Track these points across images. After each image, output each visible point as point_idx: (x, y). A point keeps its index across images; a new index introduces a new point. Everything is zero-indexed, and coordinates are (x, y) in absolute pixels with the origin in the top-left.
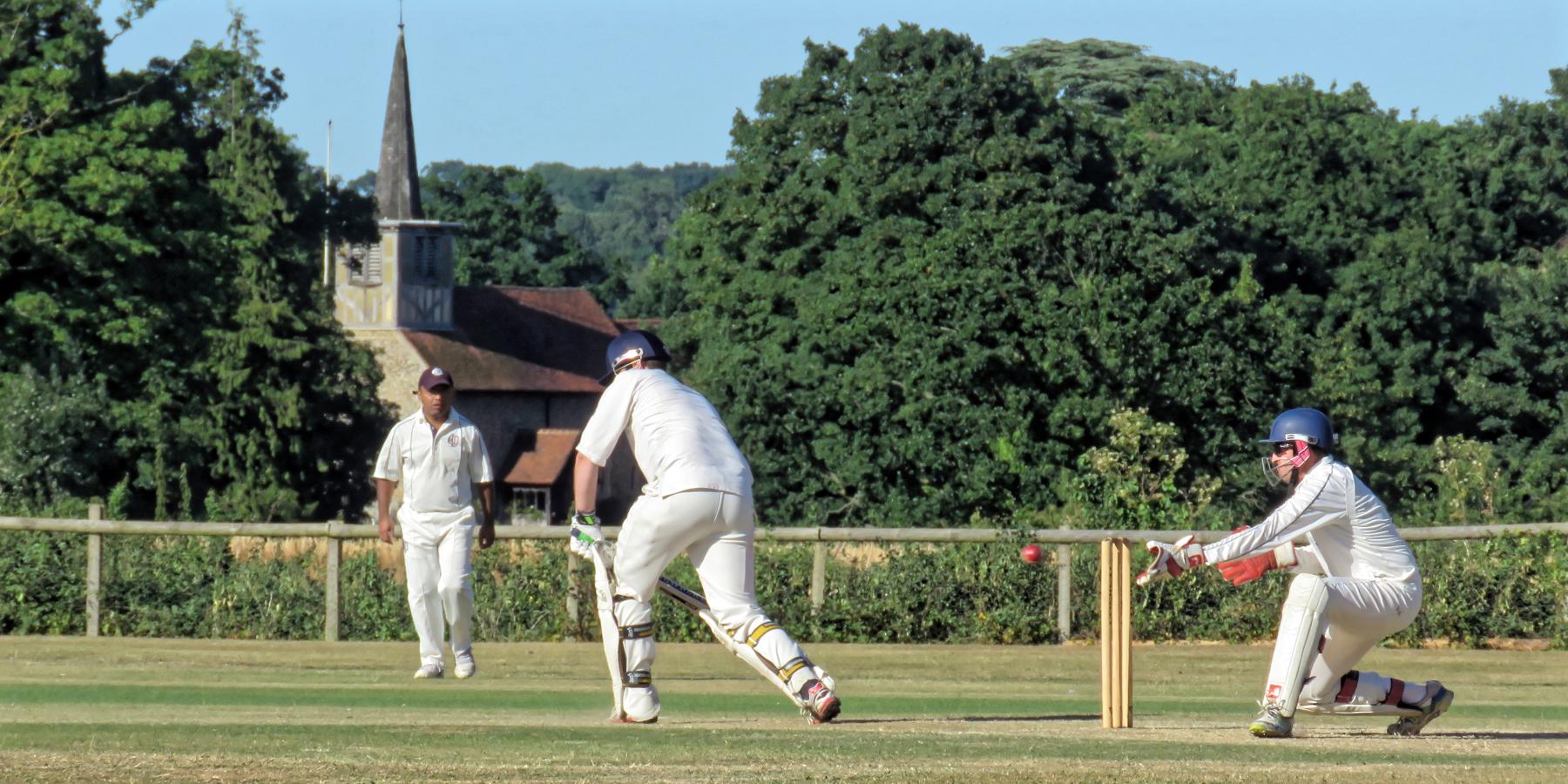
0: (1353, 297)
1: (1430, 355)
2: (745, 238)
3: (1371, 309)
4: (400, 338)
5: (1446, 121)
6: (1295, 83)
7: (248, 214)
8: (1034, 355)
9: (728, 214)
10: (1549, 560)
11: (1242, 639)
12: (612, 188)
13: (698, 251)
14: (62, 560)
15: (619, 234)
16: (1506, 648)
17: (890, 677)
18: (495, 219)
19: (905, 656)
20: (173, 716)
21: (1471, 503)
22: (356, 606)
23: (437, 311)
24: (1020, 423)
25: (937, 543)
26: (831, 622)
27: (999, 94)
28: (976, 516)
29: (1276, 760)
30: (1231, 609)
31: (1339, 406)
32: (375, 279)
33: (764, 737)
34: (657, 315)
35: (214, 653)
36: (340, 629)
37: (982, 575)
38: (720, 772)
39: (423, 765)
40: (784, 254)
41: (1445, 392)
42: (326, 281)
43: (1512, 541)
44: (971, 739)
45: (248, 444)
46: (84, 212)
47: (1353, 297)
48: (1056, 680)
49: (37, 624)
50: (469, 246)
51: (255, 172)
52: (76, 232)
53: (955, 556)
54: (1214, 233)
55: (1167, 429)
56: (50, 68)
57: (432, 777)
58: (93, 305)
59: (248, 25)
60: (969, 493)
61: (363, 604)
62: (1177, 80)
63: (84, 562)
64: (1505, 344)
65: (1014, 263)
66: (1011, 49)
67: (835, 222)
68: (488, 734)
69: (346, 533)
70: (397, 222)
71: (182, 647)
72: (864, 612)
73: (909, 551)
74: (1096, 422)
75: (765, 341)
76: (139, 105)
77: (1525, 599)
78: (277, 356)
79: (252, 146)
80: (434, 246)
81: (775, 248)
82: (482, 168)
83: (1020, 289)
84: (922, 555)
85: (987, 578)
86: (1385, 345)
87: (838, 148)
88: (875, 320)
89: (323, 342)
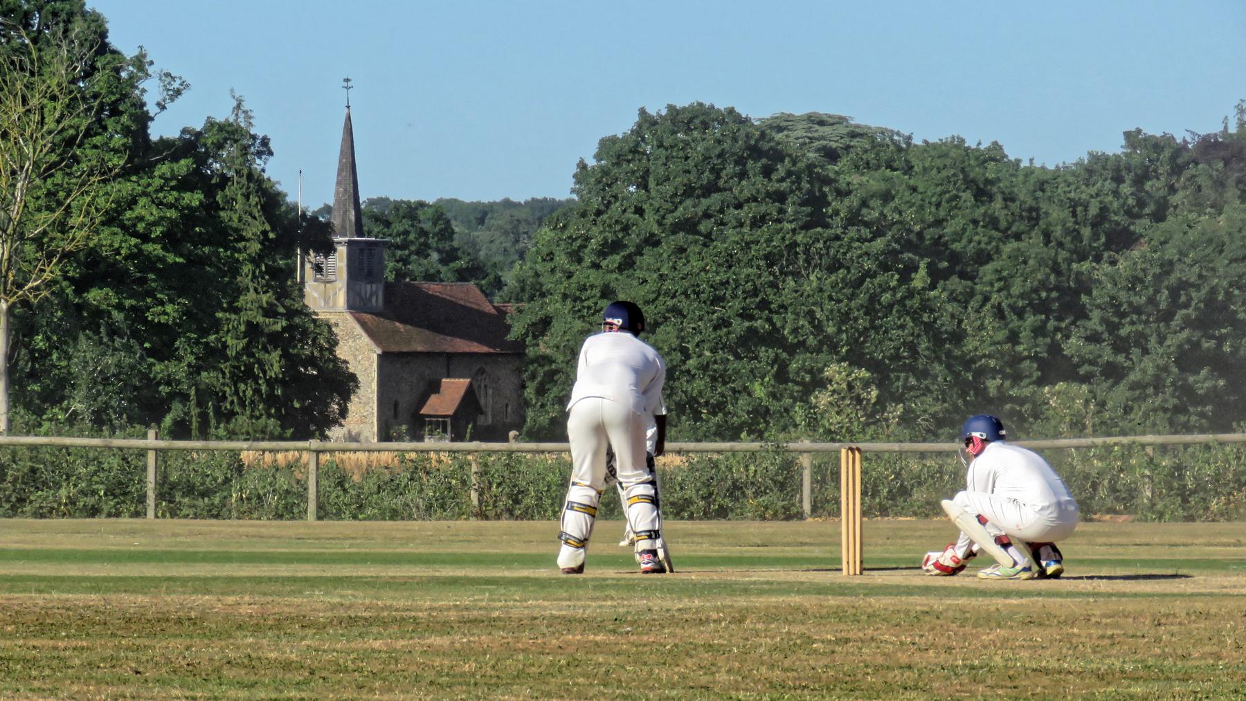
0: (992, 285)
1: (1045, 323)
2: (583, 247)
4: (349, 317)
7: (248, 234)
8: (779, 324)
9: (571, 231)
10: (1133, 461)
11: (927, 516)
12: (489, 216)
13: (551, 256)
14: (129, 467)
15: (494, 247)
16: (1104, 521)
17: (692, 543)
18: (412, 237)
20: (214, 571)
21: (1073, 425)
23: (374, 299)
24: (769, 371)
25: (719, 452)
28: (743, 435)
29: (962, 596)
31: (983, 361)
32: (333, 278)
33: (615, 582)
34: (522, 301)
35: (236, 529)
38: (589, 606)
39: (388, 603)
40: (609, 258)
41: (1055, 349)
43: (1108, 448)
44: (755, 583)
45: (247, 390)
46: (135, 234)
47: (992, 285)
48: (806, 544)
49: (114, 510)
50: (394, 255)
51: (250, 206)
52: (129, 249)
54: (897, 241)
56: (112, 137)
58: (141, 296)
59: (245, 106)
61: (334, 495)
62: (872, 140)
63: (145, 469)
64: (1096, 315)
67: (642, 237)
68: (429, 582)
69: (322, 448)
70: (346, 239)
71: (213, 526)
72: (671, 499)
76: (171, 162)
77: (1118, 487)
78: (266, 330)
79: (248, 188)
82: (402, 202)
83: (771, 282)
84: (710, 459)
85: (754, 476)
86: (1015, 317)
88: (670, 303)
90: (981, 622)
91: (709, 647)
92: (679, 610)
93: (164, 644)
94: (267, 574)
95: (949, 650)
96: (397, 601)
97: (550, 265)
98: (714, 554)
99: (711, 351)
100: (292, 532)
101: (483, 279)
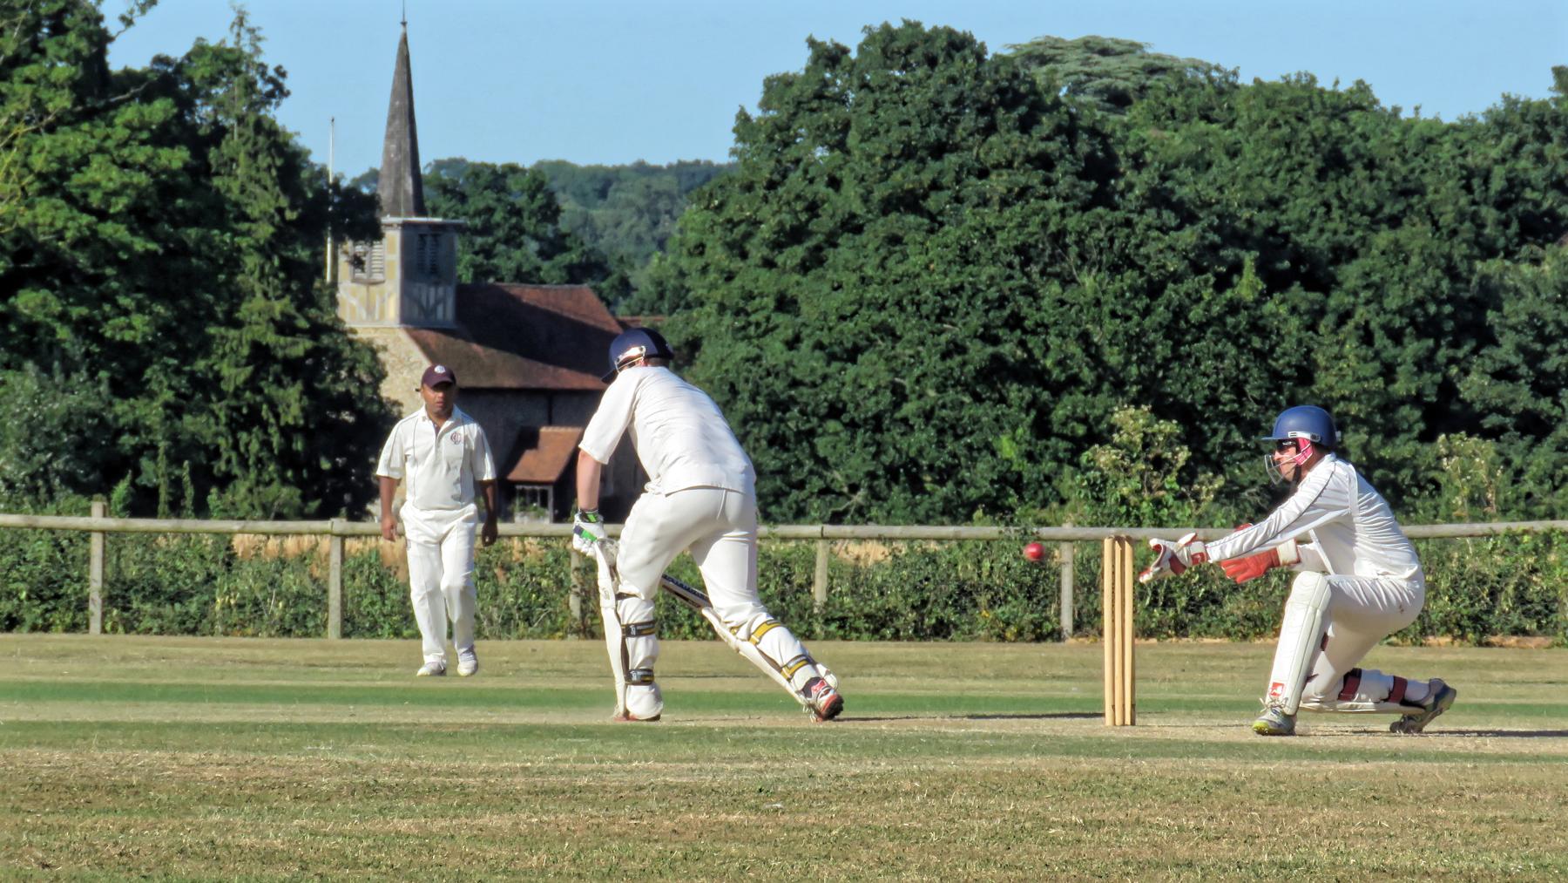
0: (1356, 294)
1: (1433, 352)
2: (748, 236)
3: (1374, 306)
4: (403, 336)
5: (1449, 118)
6: (1298, 81)
7: (253, 211)
8: (1037, 353)
9: (731, 211)
11: (1245, 637)
12: (614, 186)
13: (700, 248)
14: (64, 558)
15: (622, 231)
17: (892, 675)
18: (498, 217)
19: (907, 654)
22: (359, 604)
23: (440, 309)
25: (940, 540)
26: (833, 620)
27: (1001, 91)
28: (978, 513)
29: (1279, 758)
30: (1234, 607)
31: (1342, 404)
32: (378, 277)
34: (660, 312)
36: (343, 626)
37: (985, 573)
39: (426, 763)
40: (787, 251)
41: (1448, 389)
42: (328, 278)
43: (1514, 538)
44: (974, 736)
45: (251, 442)
46: (87, 209)
47: (1356, 294)
48: (1059, 678)
49: (40, 621)
50: (472, 244)
51: (258, 170)
52: (79, 229)
53: (958, 554)
54: (1217, 230)
55: (1170, 427)
56: (53, 65)
57: (435, 775)
59: (251, 22)
60: (972, 491)
61: (366, 602)
62: (1180, 76)
65: (1016, 261)
66: (1014, 46)
67: (838, 219)
68: (491, 732)
69: (349, 531)
70: (399, 220)
71: (185, 645)
72: (867, 610)
73: (911, 548)
74: (1099, 420)
75: (768, 339)
76: (142, 102)
77: (1528, 597)
78: (280, 354)
79: (255, 144)
80: (437, 244)
81: (777, 246)
82: (485, 166)
84: (924, 552)
85: (990, 575)
86: (1388, 342)
87: (841, 145)
88: (878, 317)
89: (325, 340)
90: (1302, 797)
91: (896, 832)
92: (855, 776)
93: (89, 822)
94: (253, 719)
95: (1250, 839)
96: (435, 760)
97: (699, 262)
98: (922, 693)
99: (938, 390)
100: (298, 656)
101: (603, 279)
